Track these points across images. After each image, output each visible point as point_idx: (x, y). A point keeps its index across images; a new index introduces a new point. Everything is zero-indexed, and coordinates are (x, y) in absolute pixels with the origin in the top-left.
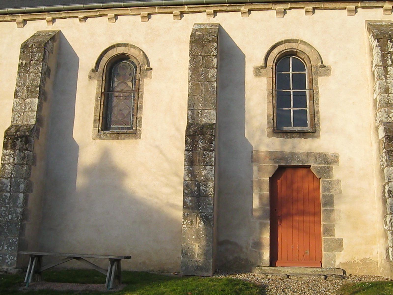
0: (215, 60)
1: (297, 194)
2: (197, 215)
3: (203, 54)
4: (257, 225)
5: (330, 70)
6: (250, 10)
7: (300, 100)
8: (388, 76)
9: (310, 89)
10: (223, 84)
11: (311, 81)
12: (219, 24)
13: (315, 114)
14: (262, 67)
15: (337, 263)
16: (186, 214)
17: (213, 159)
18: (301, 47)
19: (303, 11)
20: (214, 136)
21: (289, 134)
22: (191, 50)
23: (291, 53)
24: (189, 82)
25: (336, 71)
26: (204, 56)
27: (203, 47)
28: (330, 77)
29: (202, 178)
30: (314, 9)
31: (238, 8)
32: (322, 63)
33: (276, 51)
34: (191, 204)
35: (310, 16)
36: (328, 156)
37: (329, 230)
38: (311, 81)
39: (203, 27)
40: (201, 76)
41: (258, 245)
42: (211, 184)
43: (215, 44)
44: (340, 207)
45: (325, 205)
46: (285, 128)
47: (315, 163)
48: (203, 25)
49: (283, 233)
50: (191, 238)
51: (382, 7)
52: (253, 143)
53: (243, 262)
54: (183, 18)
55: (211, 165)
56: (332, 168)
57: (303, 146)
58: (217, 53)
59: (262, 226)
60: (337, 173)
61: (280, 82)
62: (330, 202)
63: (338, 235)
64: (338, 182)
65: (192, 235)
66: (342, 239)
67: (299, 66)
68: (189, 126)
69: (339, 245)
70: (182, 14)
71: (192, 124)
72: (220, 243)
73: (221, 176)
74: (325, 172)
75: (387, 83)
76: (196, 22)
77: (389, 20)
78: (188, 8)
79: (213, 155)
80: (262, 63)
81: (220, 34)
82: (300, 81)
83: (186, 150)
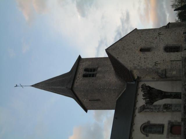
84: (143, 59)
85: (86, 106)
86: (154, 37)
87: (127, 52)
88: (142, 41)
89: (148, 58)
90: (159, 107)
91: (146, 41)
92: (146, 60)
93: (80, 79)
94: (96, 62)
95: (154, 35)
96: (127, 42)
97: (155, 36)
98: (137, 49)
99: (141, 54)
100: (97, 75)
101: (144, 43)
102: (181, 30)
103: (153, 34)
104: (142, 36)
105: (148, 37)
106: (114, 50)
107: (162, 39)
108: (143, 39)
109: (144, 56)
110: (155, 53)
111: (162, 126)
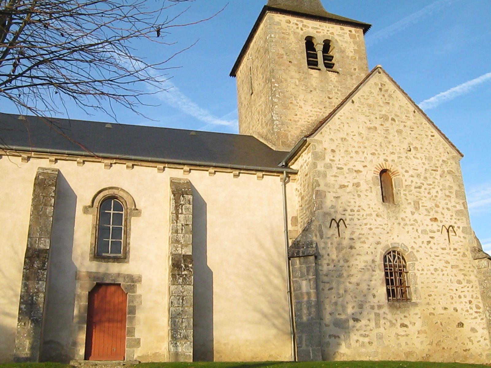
0: (53, 200)
1: (108, 305)
2: (30, 319)
3: (44, 194)
4: (77, 327)
5: (141, 213)
6: (84, 161)
7: (117, 233)
8: (178, 221)
9: (125, 226)
10: (57, 217)
11: (126, 220)
12: (59, 170)
13: (127, 244)
14: (89, 207)
15: (135, 357)
16: (21, 318)
17: (45, 276)
18: (121, 194)
19: (125, 166)
20: (48, 259)
21: (106, 260)
22: (34, 190)
23: (114, 197)
24: (31, 215)
25: (144, 213)
26: (44, 197)
27: (44, 189)
28: (140, 218)
29: (36, 290)
30: (133, 165)
31: (74, 159)
32: (135, 206)
33: (101, 195)
34: (25, 310)
35: (130, 171)
36: (134, 277)
37: (131, 332)
38: (126, 220)
39: (45, 171)
40: (41, 212)
41: (75, 344)
42: (42, 295)
43: (54, 188)
44: (140, 315)
45: (129, 313)
46: (104, 254)
47: (124, 281)
48: (46, 169)
49: (96, 336)
50: (23, 336)
51: (182, 169)
52: (77, 264)
53: (64, 357)
54: (29, 162)
55: (43, 281)
56: (136, 285)
57: (114, 268)
58: (55, 194)
59: (80, 328)
60: (140, 290)
61: (103, 217)
62: (133, 311)
63: (137, 335)
64: (140, 296)
65: (24, 334)
66: (140, 339)
67: (118, 207)
68: (28, 249)
69: (138, 342)
70: (29, 158)
71: (30, 248)
72: (46, 343)
73: (51, 290)
74: (131, 289)
75: (177, 226)
76: (40, 166)
77: (187, 179)
78: (34, 154)
79: (46, 273)
80: (90, 204)
81: (58, 180)
82: (118, 218)
83: (24, 269)
84: (356, 181)
85: (322, 130)
86: (437, 212)
87: (376, 128)
88: (418, 176)
89: (359, 196)
90: (182, 241)
91: (420, 187)
92: (348, 190)
93: (299, 31)
94: (355, 69)
95: (445, 212)
96: (412, 129)
97: (439, 217)
98: (389, 159)
99: (370, 174)
100: (314, 72)
101: (412, 181)
102: (470, 302)
103: (448, 209)
104: (439, 173)
105: (435, 194)
106: (380, 89)
107: (432, 238)
108: (426, 178)
109: (367, 182)
110: (379, 219)
111: (120, 254)
